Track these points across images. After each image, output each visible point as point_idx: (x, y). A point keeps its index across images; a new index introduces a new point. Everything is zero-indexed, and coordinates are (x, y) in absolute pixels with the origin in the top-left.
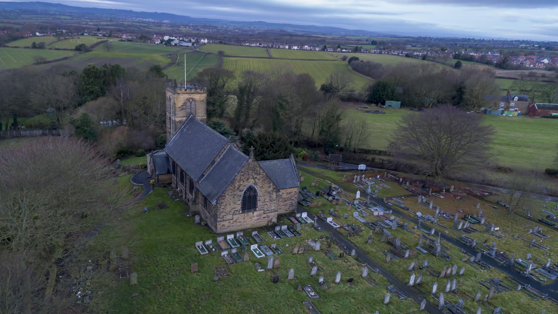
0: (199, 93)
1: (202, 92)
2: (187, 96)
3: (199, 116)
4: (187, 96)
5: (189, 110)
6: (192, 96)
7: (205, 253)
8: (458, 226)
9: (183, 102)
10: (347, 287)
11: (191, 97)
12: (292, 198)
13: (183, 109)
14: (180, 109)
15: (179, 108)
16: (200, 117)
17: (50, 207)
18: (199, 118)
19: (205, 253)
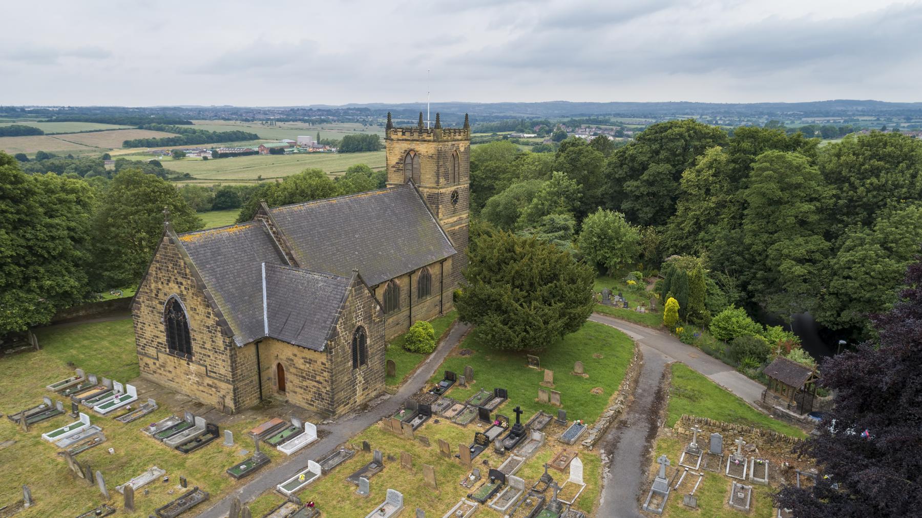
0: (425, 141)
1: (432, 138)
2: (405, 146)
3: (426, 187)
4: (405, 146)
5: (409, 174)
6: (413, 146)
7: (763, 481)
8: (260, 318)
9: (399, 157)
10: (615, 396)
11: (412, 148)
12: (318, 378)
13: (399, 170)
14: (394, 169)
15: (393, 167)
16: (428, 190)
17: (485, 512)
18: (426, 190)
19: (763, 481)
